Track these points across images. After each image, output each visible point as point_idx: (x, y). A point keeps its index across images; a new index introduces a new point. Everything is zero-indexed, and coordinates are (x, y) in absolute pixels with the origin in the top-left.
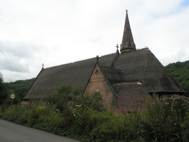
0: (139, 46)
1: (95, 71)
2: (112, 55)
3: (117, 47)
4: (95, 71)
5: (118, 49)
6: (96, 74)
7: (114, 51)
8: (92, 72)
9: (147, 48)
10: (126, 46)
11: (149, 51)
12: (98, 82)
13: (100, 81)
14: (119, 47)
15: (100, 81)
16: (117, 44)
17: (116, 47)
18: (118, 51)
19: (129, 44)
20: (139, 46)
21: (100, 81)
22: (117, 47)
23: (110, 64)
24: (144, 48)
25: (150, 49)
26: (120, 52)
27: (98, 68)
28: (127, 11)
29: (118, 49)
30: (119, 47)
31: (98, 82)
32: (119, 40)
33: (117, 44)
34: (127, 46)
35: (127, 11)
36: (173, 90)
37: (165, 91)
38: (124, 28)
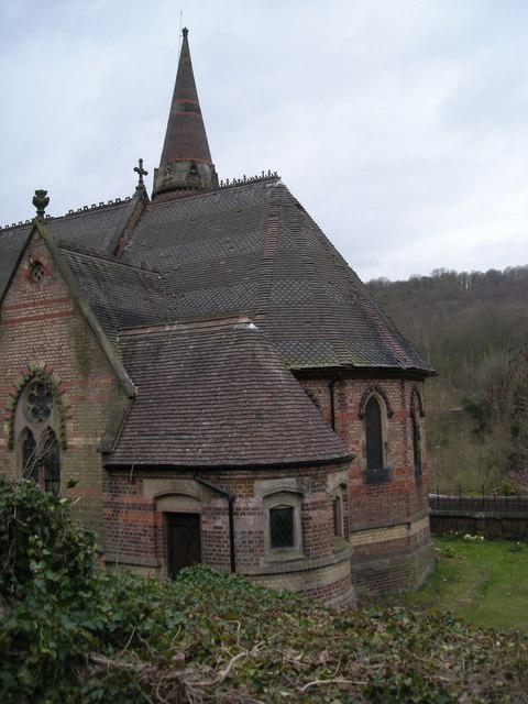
0: (231, 162)
1: (25, 266)
2: (118, 205)
3: (141, 172)
4: (25, 266)
5: (141, 182)
6: (30, 278)
7: (125, 189)
8: (13, 275)
9: (275, 178)
10: (180, 175)
11: (283, 187)
12: (39, 318)
13: (46, 316)
14: (146, 173)
15: (46, 316)
16: (141, 161)
17: (136, 169)
18: (141, 188)
19: (193, 167)
20: (231, 162)
21: (51, 316)
22: (141, 172)
23: (107, 244)
24: (260, 175)
25: (284, 181)
26: (150, 193)
27: (43, 248)
28: (185, 32)
29: (141, 182)
30: (146, 173)
31: (39, 318)
32: (151, 148)
33: (141, 161)
34: (184, 177)
35: (185, 32)
36: (390, 357)
37: (357, 365)
38: (173, 101)
